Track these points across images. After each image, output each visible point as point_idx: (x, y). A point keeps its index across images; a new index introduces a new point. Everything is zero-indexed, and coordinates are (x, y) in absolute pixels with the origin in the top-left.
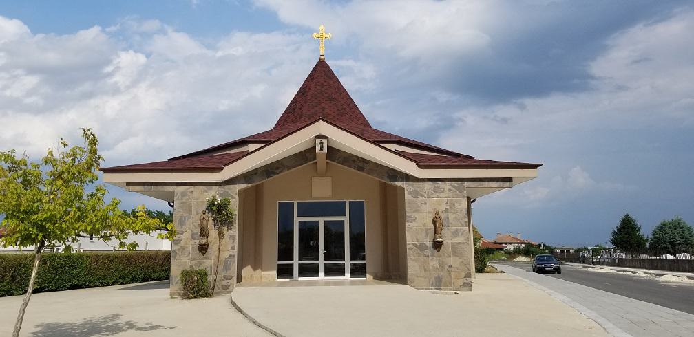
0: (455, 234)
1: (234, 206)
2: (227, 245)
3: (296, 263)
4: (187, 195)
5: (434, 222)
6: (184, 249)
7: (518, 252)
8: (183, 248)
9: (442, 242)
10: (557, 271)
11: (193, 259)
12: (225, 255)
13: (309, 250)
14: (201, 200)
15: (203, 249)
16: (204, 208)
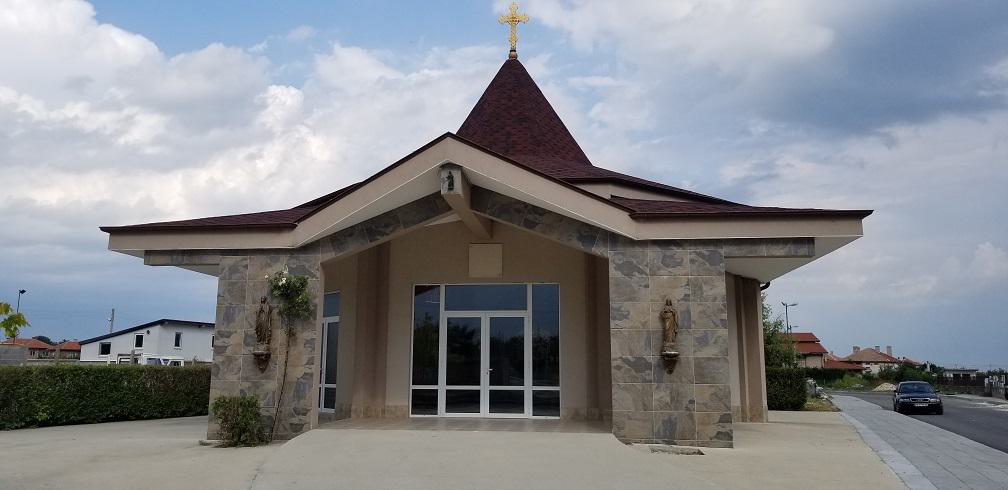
0: (703, 341)
1: (316, 288)
2: (303, 356)
3: (442, 388)
4: (237, 271)
5: (663, 319)
6: (231, 361)
7: (885, 376)
8: (230, 360)
9: (675, 356)
10: (936, 410)
11: (246, 379)
12: (297, 373)
13: (464, 368)
14: (260, 279)
15: (262, 361)
16: (265, 293)
